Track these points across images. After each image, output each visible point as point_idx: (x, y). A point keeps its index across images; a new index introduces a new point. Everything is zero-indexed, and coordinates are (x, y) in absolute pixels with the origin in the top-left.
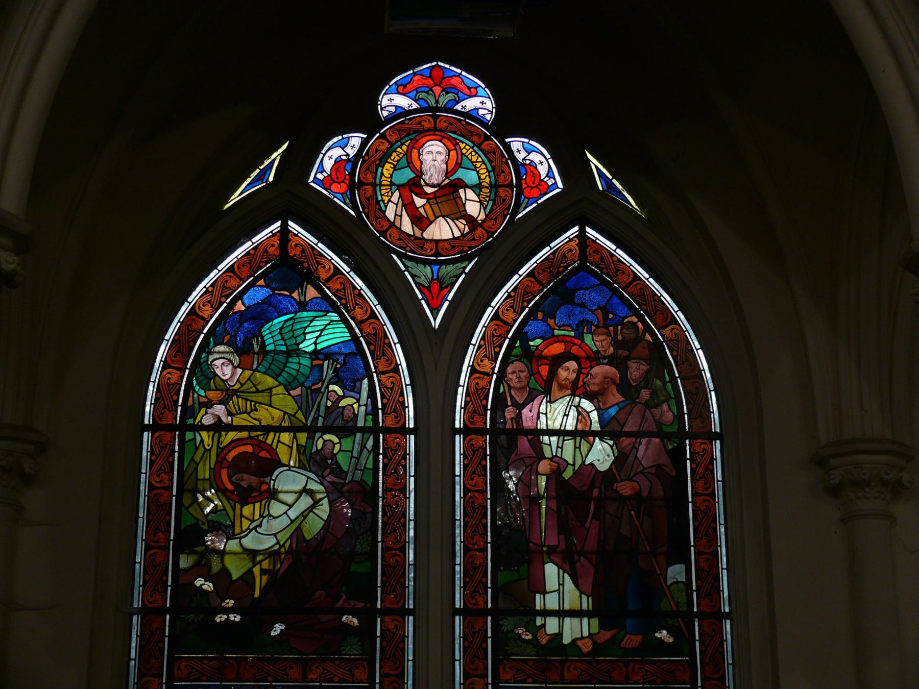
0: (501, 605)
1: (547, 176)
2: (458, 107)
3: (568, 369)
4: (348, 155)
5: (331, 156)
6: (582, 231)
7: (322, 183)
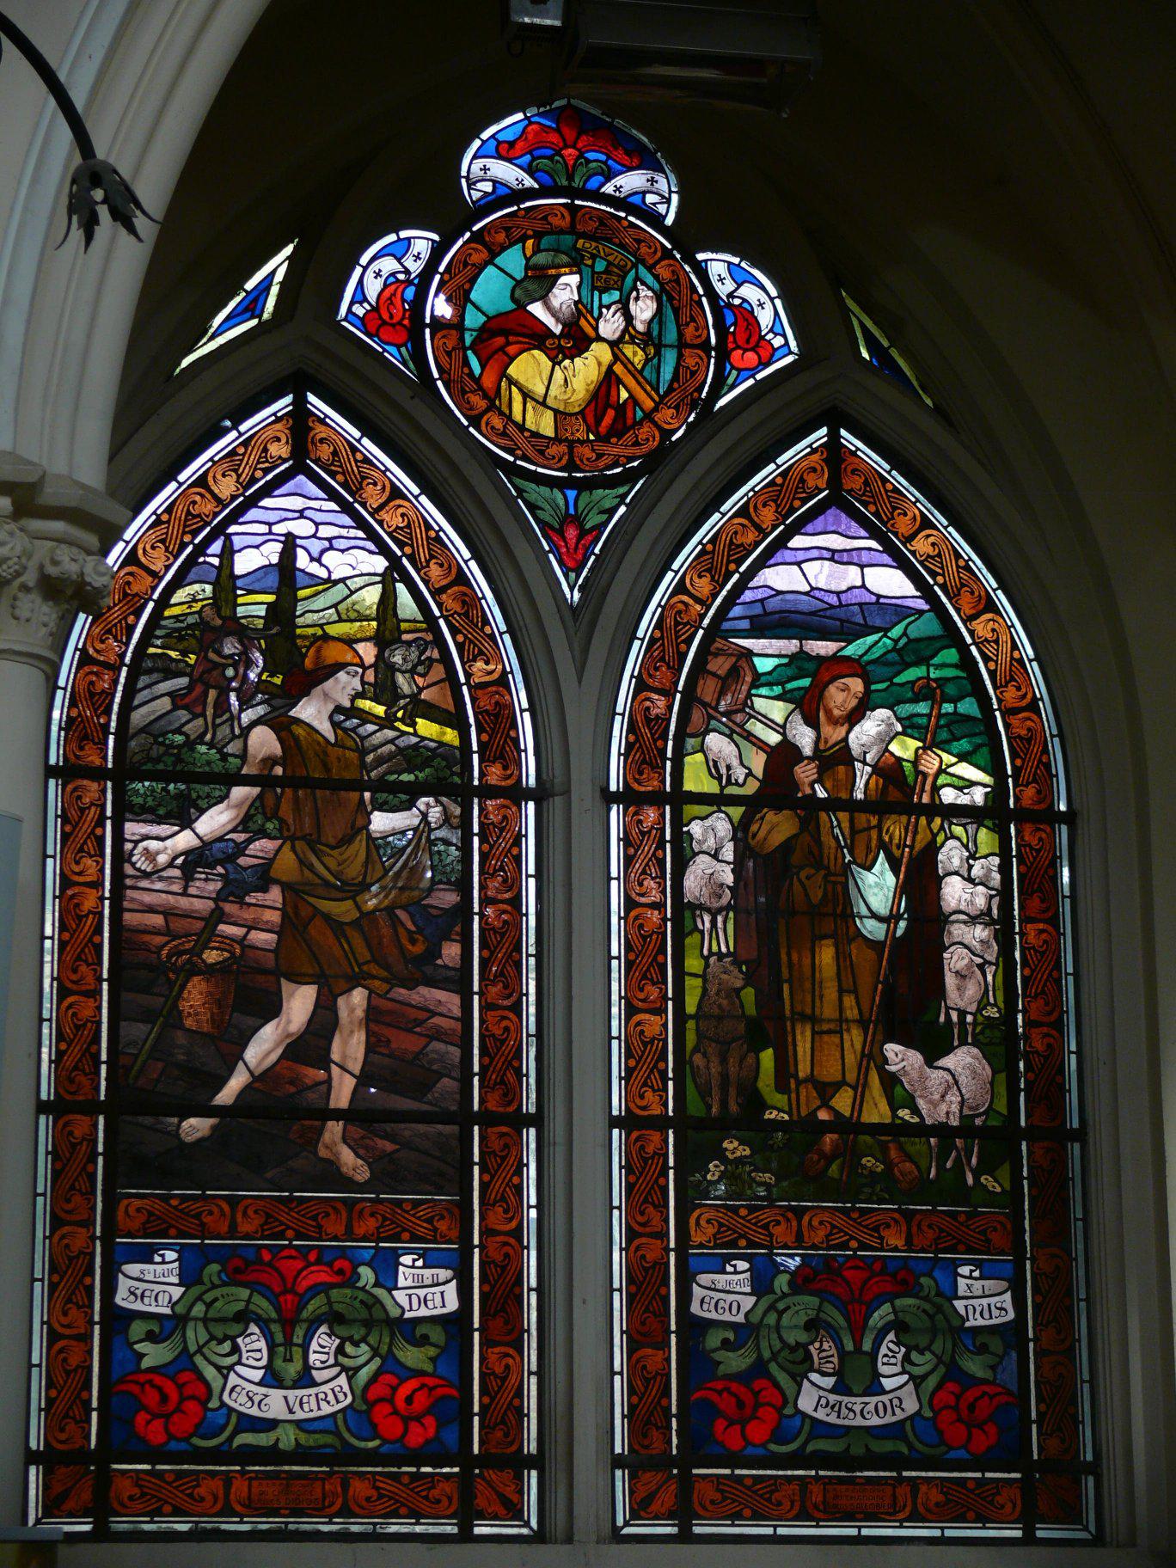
0: (491, 1106)
1: (771, 330)
2: (608, 189)
3: (846, 689)
4: (407, 272)
5: (373, 273)
6: (834, 436)
7: (363, 322)
